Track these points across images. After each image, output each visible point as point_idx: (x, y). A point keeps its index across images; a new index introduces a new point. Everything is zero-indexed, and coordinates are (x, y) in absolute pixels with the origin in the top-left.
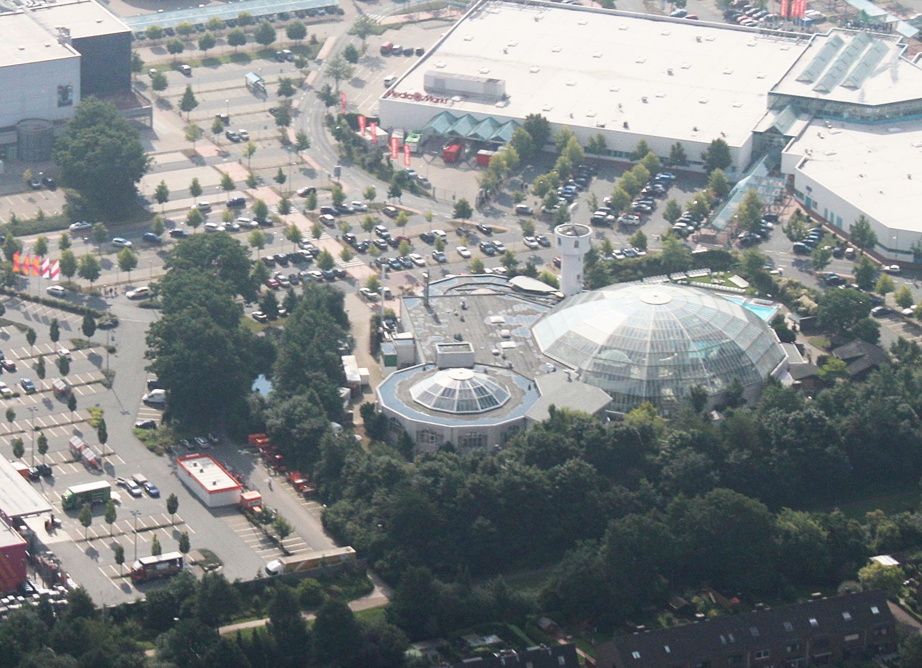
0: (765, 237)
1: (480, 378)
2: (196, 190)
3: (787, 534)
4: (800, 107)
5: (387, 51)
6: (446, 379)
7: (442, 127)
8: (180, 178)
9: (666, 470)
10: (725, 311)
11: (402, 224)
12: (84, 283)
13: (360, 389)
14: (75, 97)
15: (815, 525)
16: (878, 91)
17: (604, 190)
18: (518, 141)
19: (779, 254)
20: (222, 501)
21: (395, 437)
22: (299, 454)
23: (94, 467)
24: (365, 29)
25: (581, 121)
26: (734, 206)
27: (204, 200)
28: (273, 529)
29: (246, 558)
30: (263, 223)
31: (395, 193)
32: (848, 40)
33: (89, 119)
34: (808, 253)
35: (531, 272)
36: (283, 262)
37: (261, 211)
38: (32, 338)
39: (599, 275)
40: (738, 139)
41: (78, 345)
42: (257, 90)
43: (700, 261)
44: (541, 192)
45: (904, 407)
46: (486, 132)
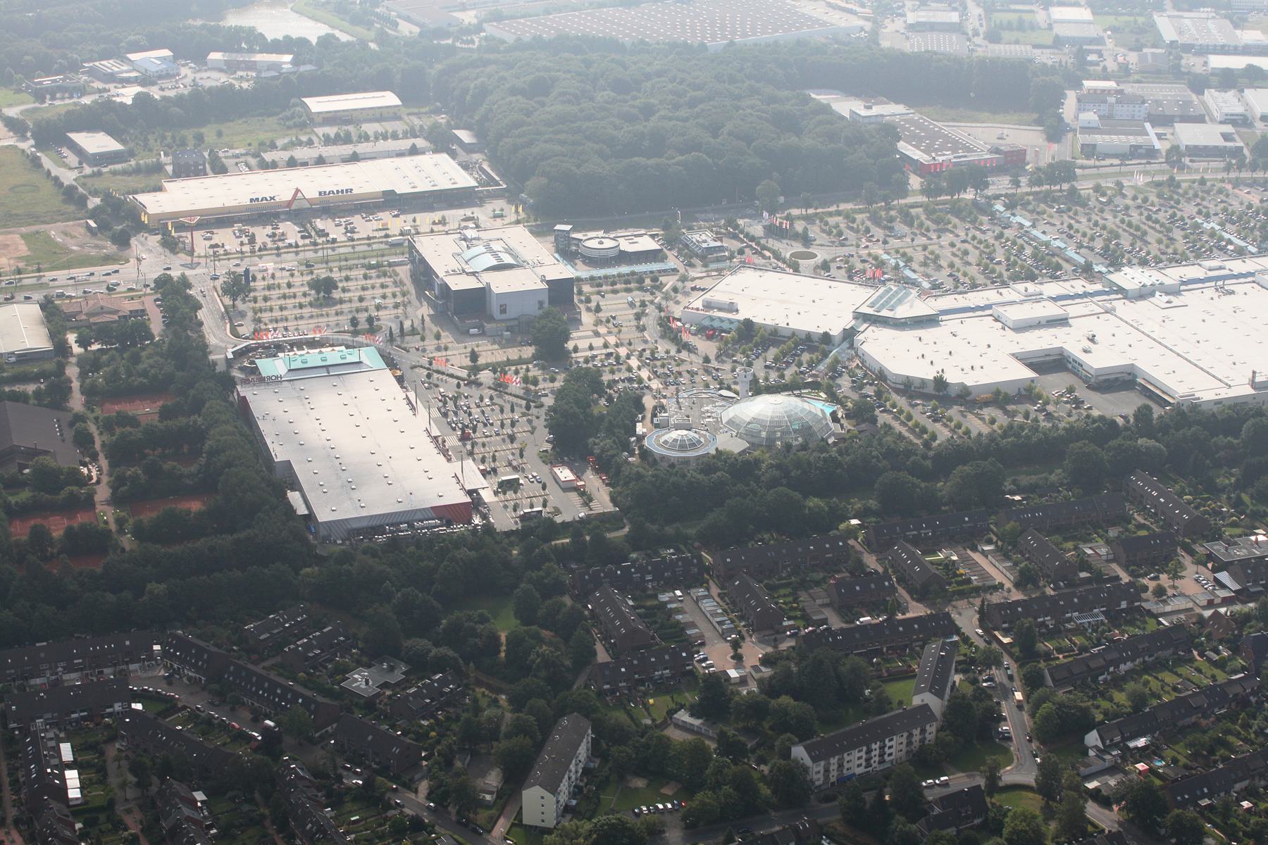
0: (840, 375)
1: (691, 434)
2: (591, 348)
3: (810, 508)
4: (866, 318)
5: (694, 289)
6: (675, 434)
7: (707, 323)
8: (585, 342)
9: (763, 478)
10: (817, 407)
11: (678, 365)
12: (532, 388)
13: (641, 438)
14: (546, 305)
15: (822, 504)
16: (902, 312)
17: (772, 352)
18: (739, 330)
19: (845, 383)
20: (569, 485)
21: (650, 459)
22: (606, 467)
23: (515, 469)
24: (684, 279)
25: (768, 322)
26: (828, 361)
27: (595, 352)
28: (587, 499)
29: (572, 510)
30: (618, 363)
31: (679, 351)
32: (895, 289)
33: (547, 315)
34: (857, 386)
35: (729, 388)
36: (623, 381)
37: (618, 358)
38: (502, 411)
39: (757, 389)
40: (836, 331)
41: (524, 415)
42: (632, 305)
43: (807, 385)
44: (743, 353)
45: (874, 453)
46: (726, 326)
